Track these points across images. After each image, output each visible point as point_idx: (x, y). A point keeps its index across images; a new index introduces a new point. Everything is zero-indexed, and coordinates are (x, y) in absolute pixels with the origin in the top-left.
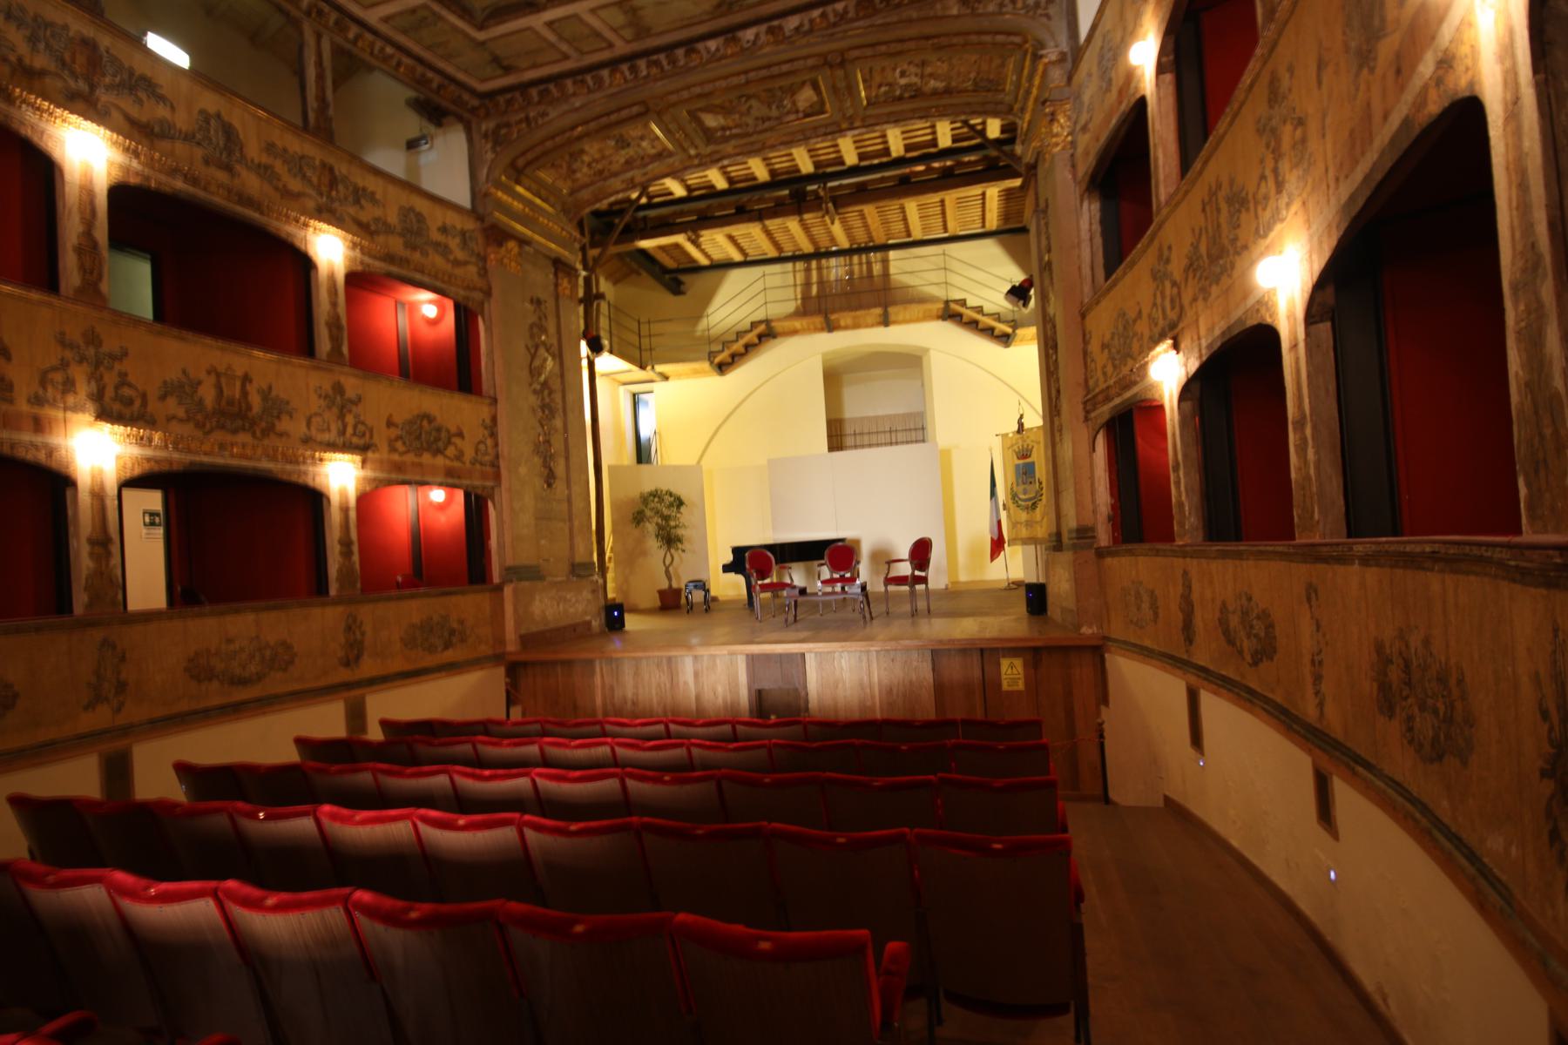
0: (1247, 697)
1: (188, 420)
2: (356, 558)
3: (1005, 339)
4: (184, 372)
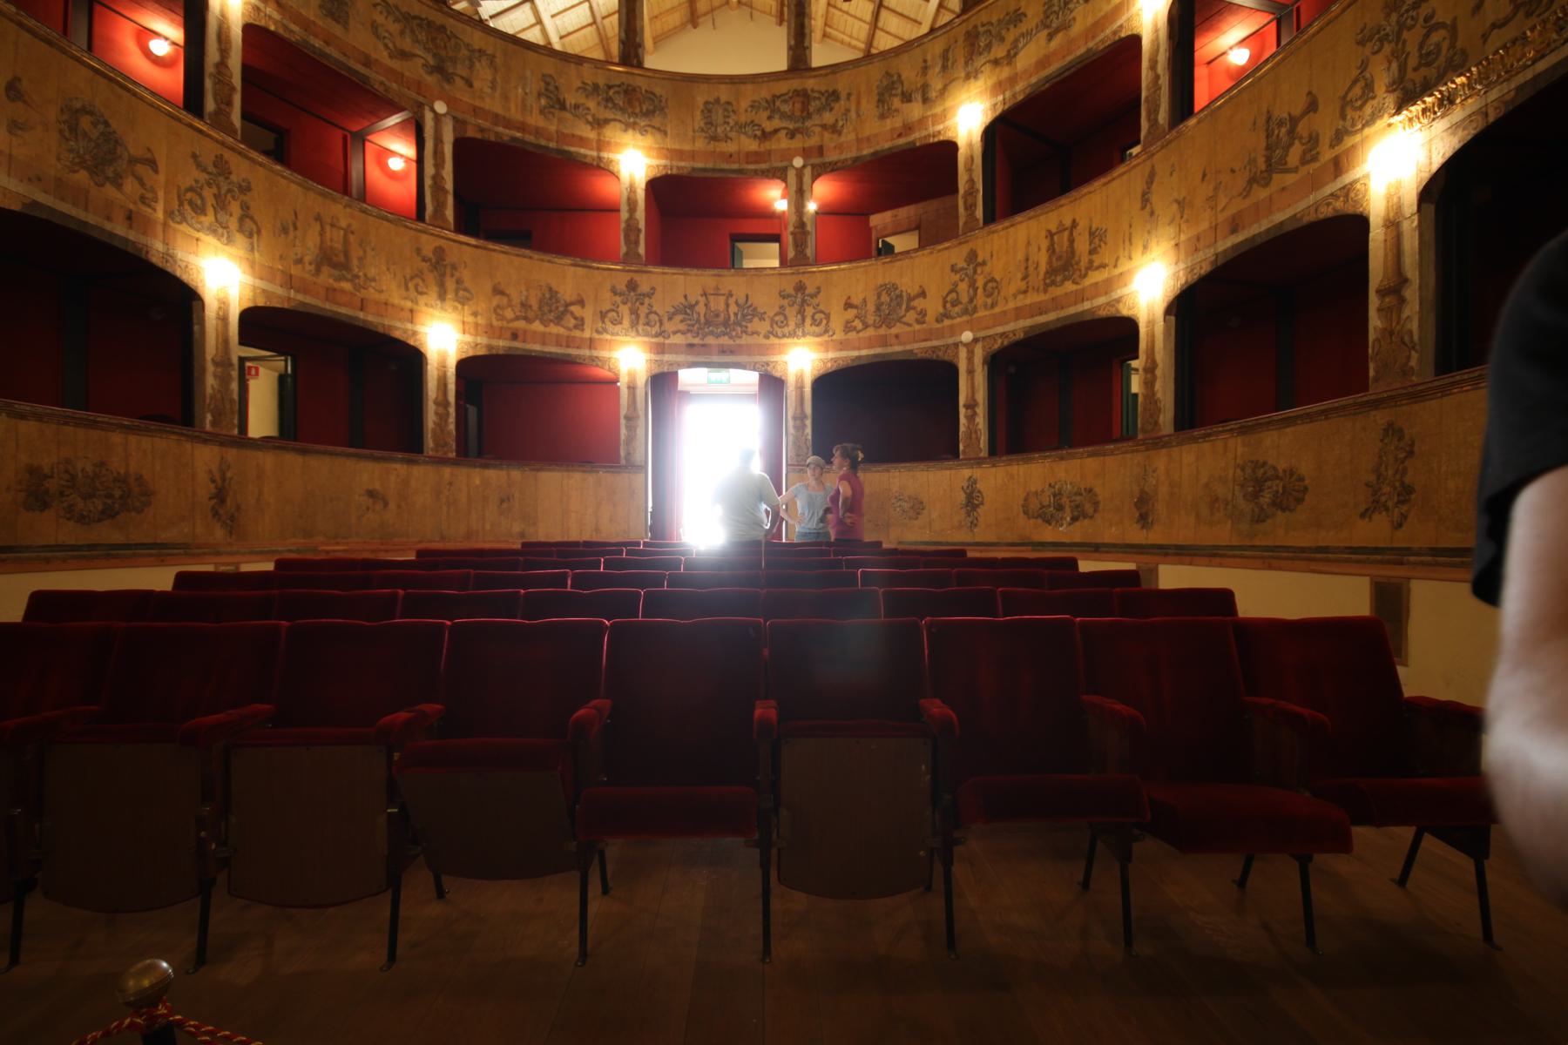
4: (685, 297)
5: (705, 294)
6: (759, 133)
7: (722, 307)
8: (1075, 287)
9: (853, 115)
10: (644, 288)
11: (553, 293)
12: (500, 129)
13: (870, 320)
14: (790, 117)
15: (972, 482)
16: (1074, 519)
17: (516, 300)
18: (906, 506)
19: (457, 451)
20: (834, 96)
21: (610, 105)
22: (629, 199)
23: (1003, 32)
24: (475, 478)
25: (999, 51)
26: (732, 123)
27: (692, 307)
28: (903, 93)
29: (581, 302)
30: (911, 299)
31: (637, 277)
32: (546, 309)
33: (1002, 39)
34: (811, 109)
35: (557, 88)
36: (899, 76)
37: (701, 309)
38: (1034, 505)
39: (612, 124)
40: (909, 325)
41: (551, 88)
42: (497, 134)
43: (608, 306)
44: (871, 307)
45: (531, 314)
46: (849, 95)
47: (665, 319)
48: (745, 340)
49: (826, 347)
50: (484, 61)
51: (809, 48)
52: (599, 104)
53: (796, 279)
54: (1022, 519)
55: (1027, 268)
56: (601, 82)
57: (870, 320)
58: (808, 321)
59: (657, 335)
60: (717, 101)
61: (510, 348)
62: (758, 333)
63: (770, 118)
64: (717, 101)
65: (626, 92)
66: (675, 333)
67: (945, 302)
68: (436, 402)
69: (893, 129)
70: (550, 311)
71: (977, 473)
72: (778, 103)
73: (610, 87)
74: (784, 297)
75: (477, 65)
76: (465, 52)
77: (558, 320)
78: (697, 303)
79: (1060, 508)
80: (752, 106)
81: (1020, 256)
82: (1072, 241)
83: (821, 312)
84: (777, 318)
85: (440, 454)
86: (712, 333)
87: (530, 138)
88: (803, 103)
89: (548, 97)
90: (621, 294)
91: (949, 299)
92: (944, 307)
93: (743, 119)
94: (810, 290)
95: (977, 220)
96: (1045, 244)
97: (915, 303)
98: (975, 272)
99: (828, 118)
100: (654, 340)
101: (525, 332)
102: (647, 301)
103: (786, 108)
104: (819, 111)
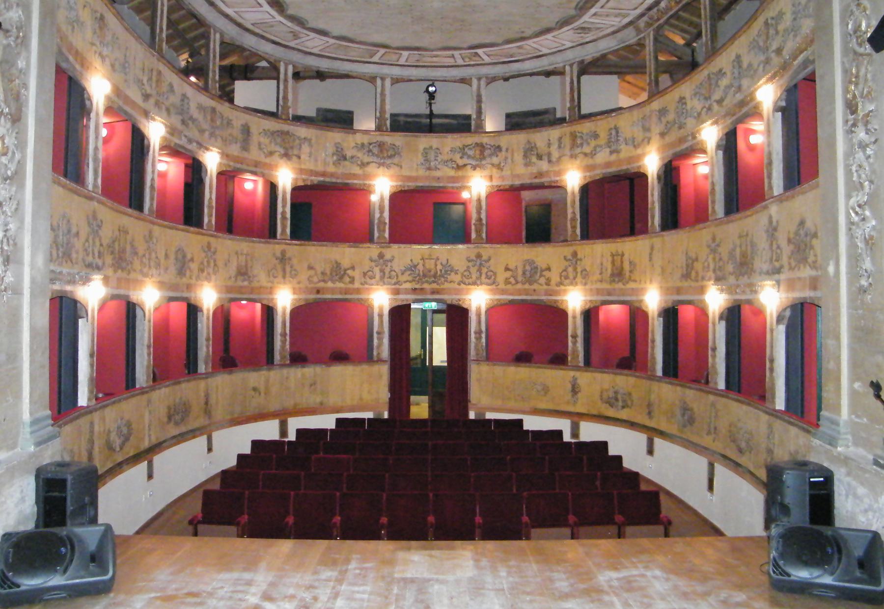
0: (736, 466)
1: (413, 281)
2: (484, 340)
3: (124, 189)
4: (411, 260)
5: (423, 259)
6: (455, 166)
7: (433, 267)
8: (623, 287)
9: (509, 160)
10: (388, 256)
11: (338, 264)
12: (313, 178)
13: (520, 279)
14: (473, 158)
15: (575, 379)
16: (623, 407)
17: (319, 272)
18: (540, 388)
19: (290, 360)
20: (499, 148)
21: (370, 154)
22: (380, 206)
23: (589, 140)
24: (298, 373)
25: (587, 149)
26: (439, 160)
27: (415, 266)
28: (537, 154)
29: (353, 268)
30: (542, 271)
31: (384, 250)
32: (334, 274)
33: (588, 144)
34: (485, 154)
35: (342, 149)
36: (535, 145)
37: (420, 267)
38: (605, 396)
39: (371, 164)
40: (541, 285)
41: (339, 150)
42: (312, 180)
43: (366, 269)
44: (520, 272)
45: (326, 278)
46: (507, 150)
47: (400, 275)
48: (446, 285)
49: (493, 292)
50: (306, 144)
51: (484, 120)
52: (364, 154)
53: (476, 251)
54: (599, 403)
55: (602, 269)
56: (366, 142)
57: (520, 279)
58: (484, 276)
59: (395, 284)
60: (431, 147)
61: (316, 299)
62: (454, 282)
63: (461, 158)
64: (431, 147)
65: (379, 146)
66: (405, 282)
67: (561, 276)
68: (281, 335)
69: (532, 174)
70: (336, 275)
71: (578, 374)
72: (466, 149)
73: (370, 144)
74: (469, 261)
75: (303, 146)
76: (297, 142)
77: (341, 279)
78: (418, 264)
79: (617, 400)
80: (451, 151)
81: (598, 261)
82: (622, 262)
83: (492, 271)
84: (465, 273)
85: (282, 363)
86: (427, 282)
87: (328, 180)
88: (481, 151)
89: (338, 155)
90: (375, 261)
91: (563, 274)
92: (561, 278)
93: (446, 158)
94: (485, 257)
95: (577, 235)
96: (610, 259)
97: (544, 273)
98: (576, 263)
99: (495, 160)
100: (393, 287)
101: (323, 288)
102: (389, 264)
103: (471, 153)
104: (491, 155)
